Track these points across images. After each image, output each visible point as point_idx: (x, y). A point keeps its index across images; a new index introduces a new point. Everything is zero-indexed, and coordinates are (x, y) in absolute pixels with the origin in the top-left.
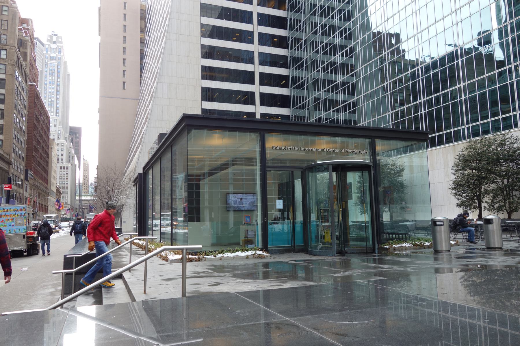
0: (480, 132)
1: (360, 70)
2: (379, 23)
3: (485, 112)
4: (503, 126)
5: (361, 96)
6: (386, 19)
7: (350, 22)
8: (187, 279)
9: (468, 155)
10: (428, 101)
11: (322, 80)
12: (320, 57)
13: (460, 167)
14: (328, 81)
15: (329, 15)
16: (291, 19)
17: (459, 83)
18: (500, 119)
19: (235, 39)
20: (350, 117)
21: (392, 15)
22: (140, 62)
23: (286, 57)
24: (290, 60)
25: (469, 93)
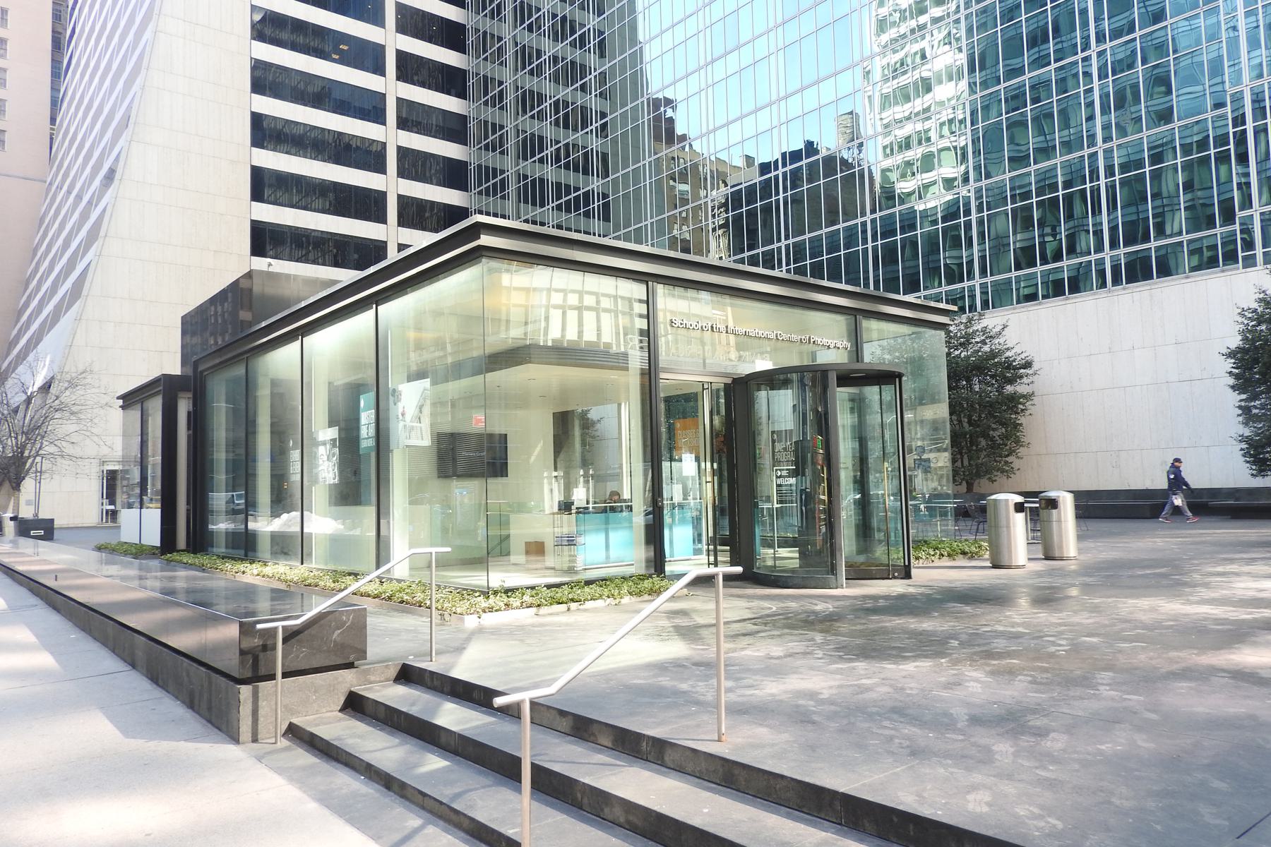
1: (644, 165)
2: (668, 79)
3: (1129, 219)
5: (646, 223)
6: (709, 59)
7: (601, 70)
9: (889, 361)
11: (552, 183)
12: (548, 130)
16: (477, 30)
18: (1187, 234)
19: (337, 57)
21: (685, 73)
22: (52, 83)
23: (463, 119)
24: (472, 125)
25: (884, 236)
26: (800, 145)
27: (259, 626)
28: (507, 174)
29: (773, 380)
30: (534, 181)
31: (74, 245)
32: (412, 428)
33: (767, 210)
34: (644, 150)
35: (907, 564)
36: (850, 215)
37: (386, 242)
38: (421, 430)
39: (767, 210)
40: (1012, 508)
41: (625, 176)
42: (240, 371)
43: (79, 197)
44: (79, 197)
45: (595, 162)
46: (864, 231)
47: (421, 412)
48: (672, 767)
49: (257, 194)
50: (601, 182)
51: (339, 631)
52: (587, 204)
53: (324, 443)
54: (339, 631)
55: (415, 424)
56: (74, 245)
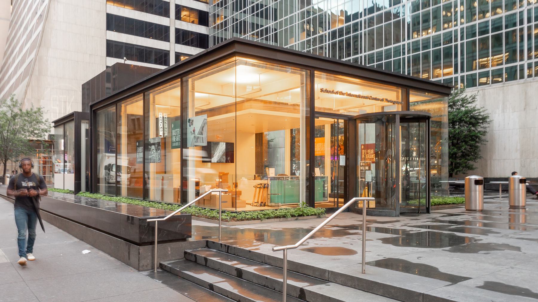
0: (351, 53)
4: (377, 55)
8: (370, 207)
10: (357, 53)
13: (479, 124)
14: (262, 17)
15: (241, 9)
17: (409, 44)
20: (262, 21)
26: (371, 5)
27: (148, 220)
28: (228, 18)
29: (367, 118)
30: (241, 22)
31: (24, 51)
32: (198, 138)
33: (292, 28)
34: (295, 7)
35: (427, 207)
36: (397, 40)
37: (169, 51)
38: (203, 138)
39: (292, 28)
40: (473, 182)
41: (286, 20)
42: (113, 109)
43: (26, 28)
44: (26, 28)
45: (271, 14)
46: (404, 49)
47: (202, 130)
48: (341, 283)
49: (109, 27)
50: (274, 23)
51: (180, 225)
52: (267, 33)
53: (154, 144)
54: (180, 225)
55: (200, 136)
56: (24, 51)
